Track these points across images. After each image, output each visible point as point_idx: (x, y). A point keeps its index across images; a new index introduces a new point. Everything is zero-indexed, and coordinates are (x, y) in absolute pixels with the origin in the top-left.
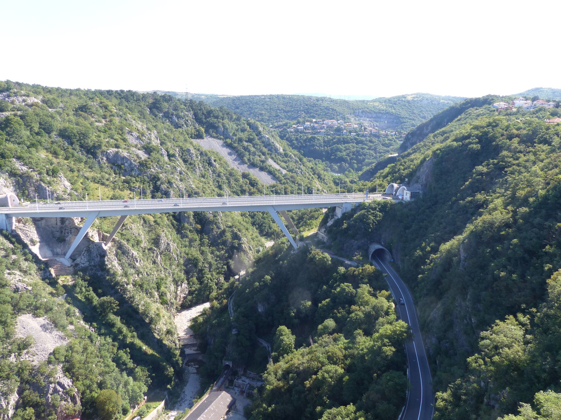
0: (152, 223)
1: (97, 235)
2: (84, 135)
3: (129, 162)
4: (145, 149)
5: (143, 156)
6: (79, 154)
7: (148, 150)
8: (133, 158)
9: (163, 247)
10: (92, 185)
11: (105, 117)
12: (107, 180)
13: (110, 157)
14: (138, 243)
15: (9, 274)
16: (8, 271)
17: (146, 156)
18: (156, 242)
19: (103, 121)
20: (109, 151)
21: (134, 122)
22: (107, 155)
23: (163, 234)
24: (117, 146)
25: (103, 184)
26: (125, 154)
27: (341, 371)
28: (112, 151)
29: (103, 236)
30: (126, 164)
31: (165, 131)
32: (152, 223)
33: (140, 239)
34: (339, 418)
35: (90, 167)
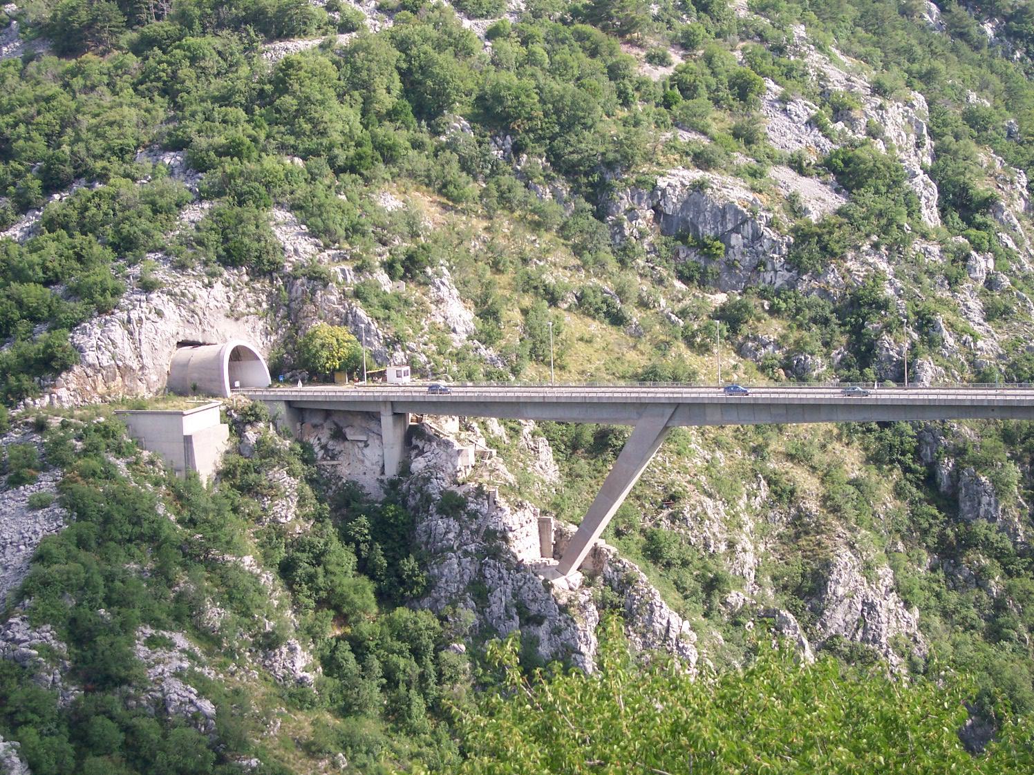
0: (813, 506)
1: (534, 528)
2: (569, 119)
3: (748, 229)
4: (840, 175)
5: (820, 200)
6: (549, 196)
7: (846, 173)
8: (768, 209)
9: (838, 619)
10: (574, 324)
11: (686, 44)
12: (643, 304)
13: (669, 209)
14: (712, 585)
15: (151, 642)
16: (149, 631)
17: (837, 201)
18: (810, 590)
19: (676, 58)
20: (662, 183)
21: (814, 57)
22: (657, 199)
23: (844, 557)
24: (702, 160)
25: (617, 320)
26: (736, 193)
27: (615, 617)
28: (677, 179)
29: (560, 534)
30: (736, 240)
31: (973, 97)
32: (813, 506)
33: (725, 567)
34: (611, 771)
35: (578, 251)
